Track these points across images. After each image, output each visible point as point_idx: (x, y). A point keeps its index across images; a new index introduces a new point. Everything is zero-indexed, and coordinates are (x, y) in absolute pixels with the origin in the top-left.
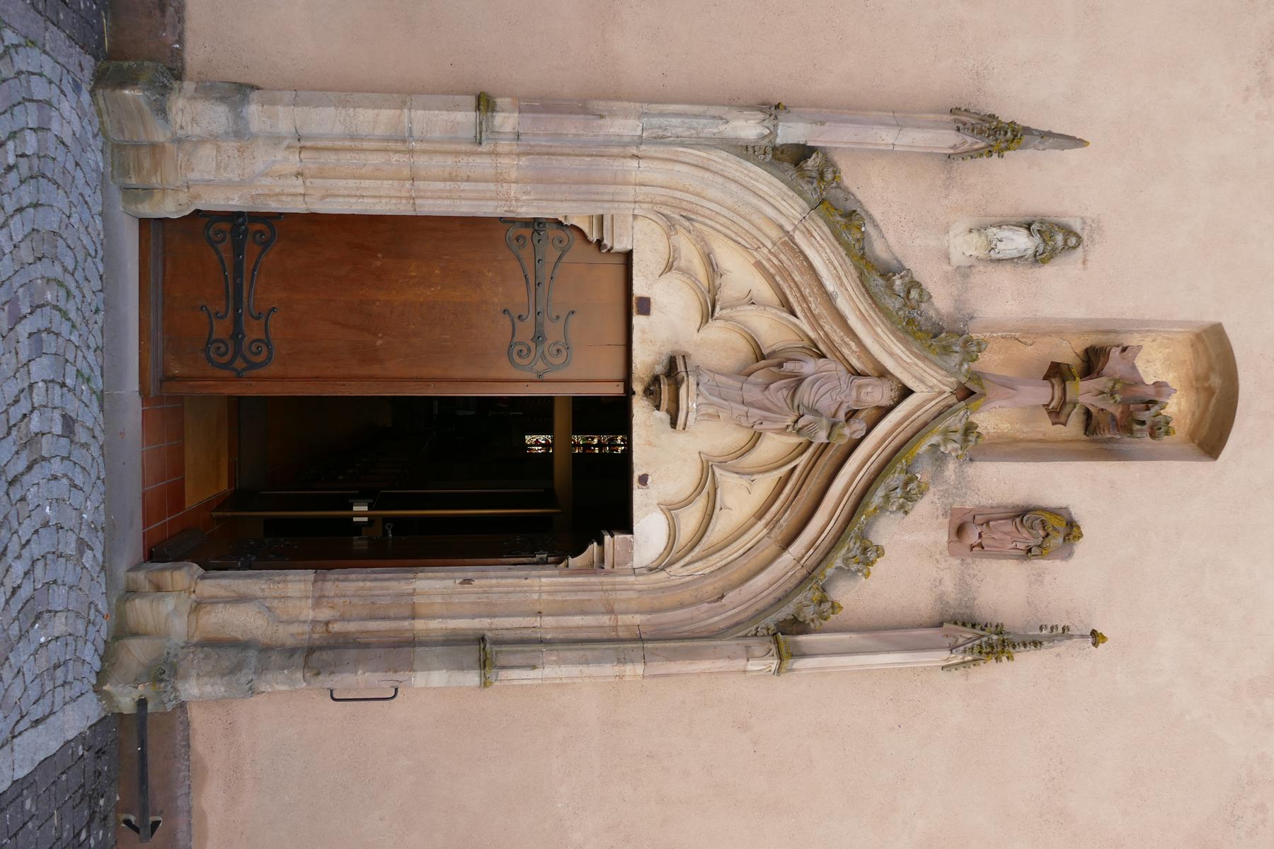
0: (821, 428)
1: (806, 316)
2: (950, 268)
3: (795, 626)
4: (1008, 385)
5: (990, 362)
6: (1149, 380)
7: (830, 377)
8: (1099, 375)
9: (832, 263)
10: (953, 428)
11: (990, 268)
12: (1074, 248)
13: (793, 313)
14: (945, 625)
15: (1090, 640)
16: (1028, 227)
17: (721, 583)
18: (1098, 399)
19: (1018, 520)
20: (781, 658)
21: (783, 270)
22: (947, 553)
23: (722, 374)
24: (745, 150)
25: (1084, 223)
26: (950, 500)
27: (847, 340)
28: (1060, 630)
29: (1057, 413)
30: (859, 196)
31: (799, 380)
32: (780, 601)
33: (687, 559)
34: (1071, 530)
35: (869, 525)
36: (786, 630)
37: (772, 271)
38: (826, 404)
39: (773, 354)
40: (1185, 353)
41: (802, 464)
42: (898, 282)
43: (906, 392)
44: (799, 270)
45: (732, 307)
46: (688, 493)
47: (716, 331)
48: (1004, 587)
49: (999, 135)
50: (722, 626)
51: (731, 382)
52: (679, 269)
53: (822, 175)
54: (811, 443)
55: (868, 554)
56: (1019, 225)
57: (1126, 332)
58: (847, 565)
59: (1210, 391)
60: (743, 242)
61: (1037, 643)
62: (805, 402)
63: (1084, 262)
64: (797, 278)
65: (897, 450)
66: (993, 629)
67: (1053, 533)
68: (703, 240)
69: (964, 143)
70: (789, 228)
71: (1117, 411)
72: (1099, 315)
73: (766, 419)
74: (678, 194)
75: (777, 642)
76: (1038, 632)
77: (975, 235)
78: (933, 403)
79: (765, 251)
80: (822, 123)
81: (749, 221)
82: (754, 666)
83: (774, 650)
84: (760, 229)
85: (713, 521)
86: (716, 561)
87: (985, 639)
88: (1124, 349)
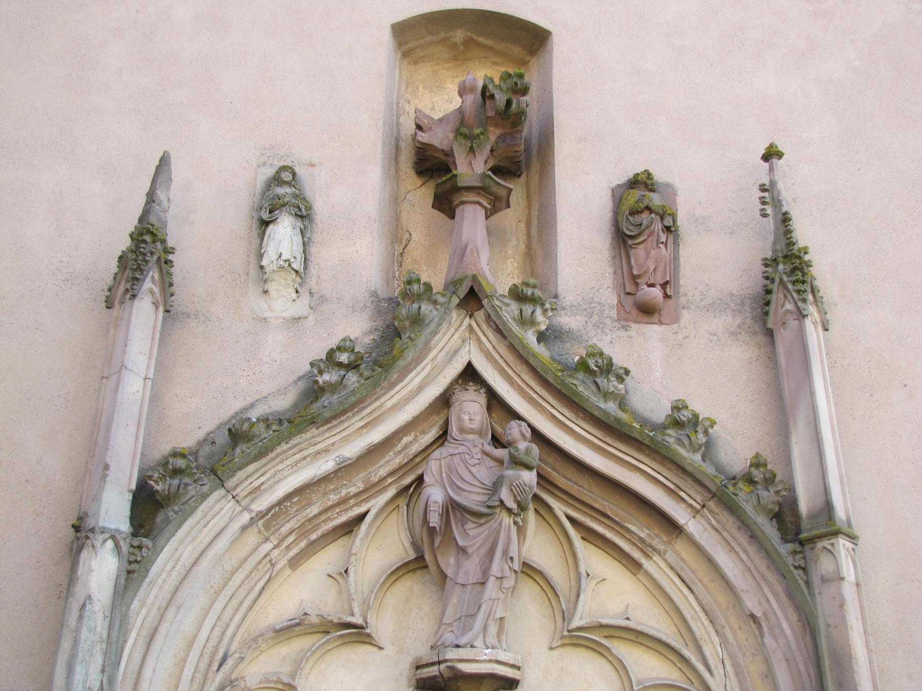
0: (519, 476)
1: (367, 500)
2: (311, 318)
3: (785, 516)
4: (461, 253)
5: (435, 276)
6: (457, 102)
7: (449, 468)
8: (449, 154)
9: (297, 463)
10: (517, 312)
11: (313, 270)
12: (294, 174)
13: (361, 517)
14: (770, 325)
15: (775, 160)
16: (265, 224)
17: (733, 619)
18: (483, 151)
19: (630, 242)
20: (836, 533)
21: (302, 530)
22: (675, 326)
23: (443, 614)
24: (133, 572)
25: (264, 164)
26: (608, 321)
27: (399, 447)
28: (766, 194)
29: (496, 204)
30: (210, 426)
31: (452, 508)
32: (754, 536)
33: (701, 668)
34: (642, 182)
35: (644, 422)
36: (794, 532)
37: (303, 544)
38: (484, 473)
39: (416, 545)
40: (424, 71)
41: (564, 508)
42: (326, 377)
43: (470, 374)
44: (304, 508)
45: (350, 600)
46: (608, 668)
47: (382, 626)
48: (715, 258)
49: (146, 253)
50: (794, 616)
51: (454, 600)
52: (293, 675)
53: (177, 472)
54: (536, 497)
55: (682, 421)
56: (262, 235)
57: (398, 130)
58: (700, 446)
59: (469, 43)
60: (261, 584)
61: (785, 219)
62: (484, 498)
63: (312, 165)
64: (314, 510)
65: (545, 383)
66: (769, 269)
67: (646, 203)
68: (255, 640)
69: (152, 292)
70: (246, 518)
71: (494, 134)
72: (379, 150)
73: (505, 552)
74: (187, 674)
75: (812, 540)
76: (770, 219)
77: (271, 287)
78: (483, 339)
79: (276, 552)
80: (107, 467)
81: (233, 573)
82: (848, 570)
83: (825, 543)
84: (246, 559)
85: (646, 630)
86: (701, 626)
87: (785, 278)
88: (419, 127)
